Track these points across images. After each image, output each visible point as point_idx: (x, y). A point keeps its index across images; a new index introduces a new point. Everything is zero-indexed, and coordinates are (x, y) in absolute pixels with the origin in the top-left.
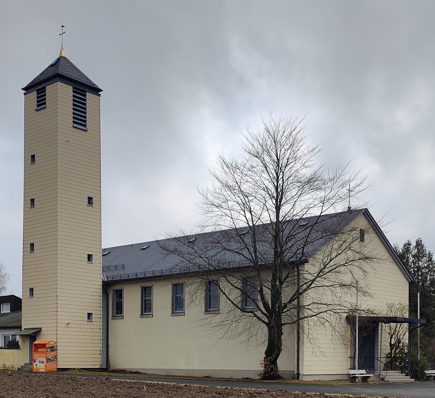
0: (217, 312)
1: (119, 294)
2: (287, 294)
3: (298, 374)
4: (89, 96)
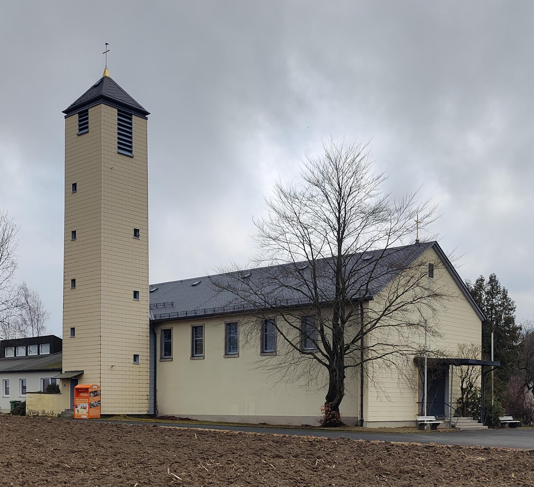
0: (274, 353)
1: (168, 334)
2: (349, 334)
4: (136, 119)
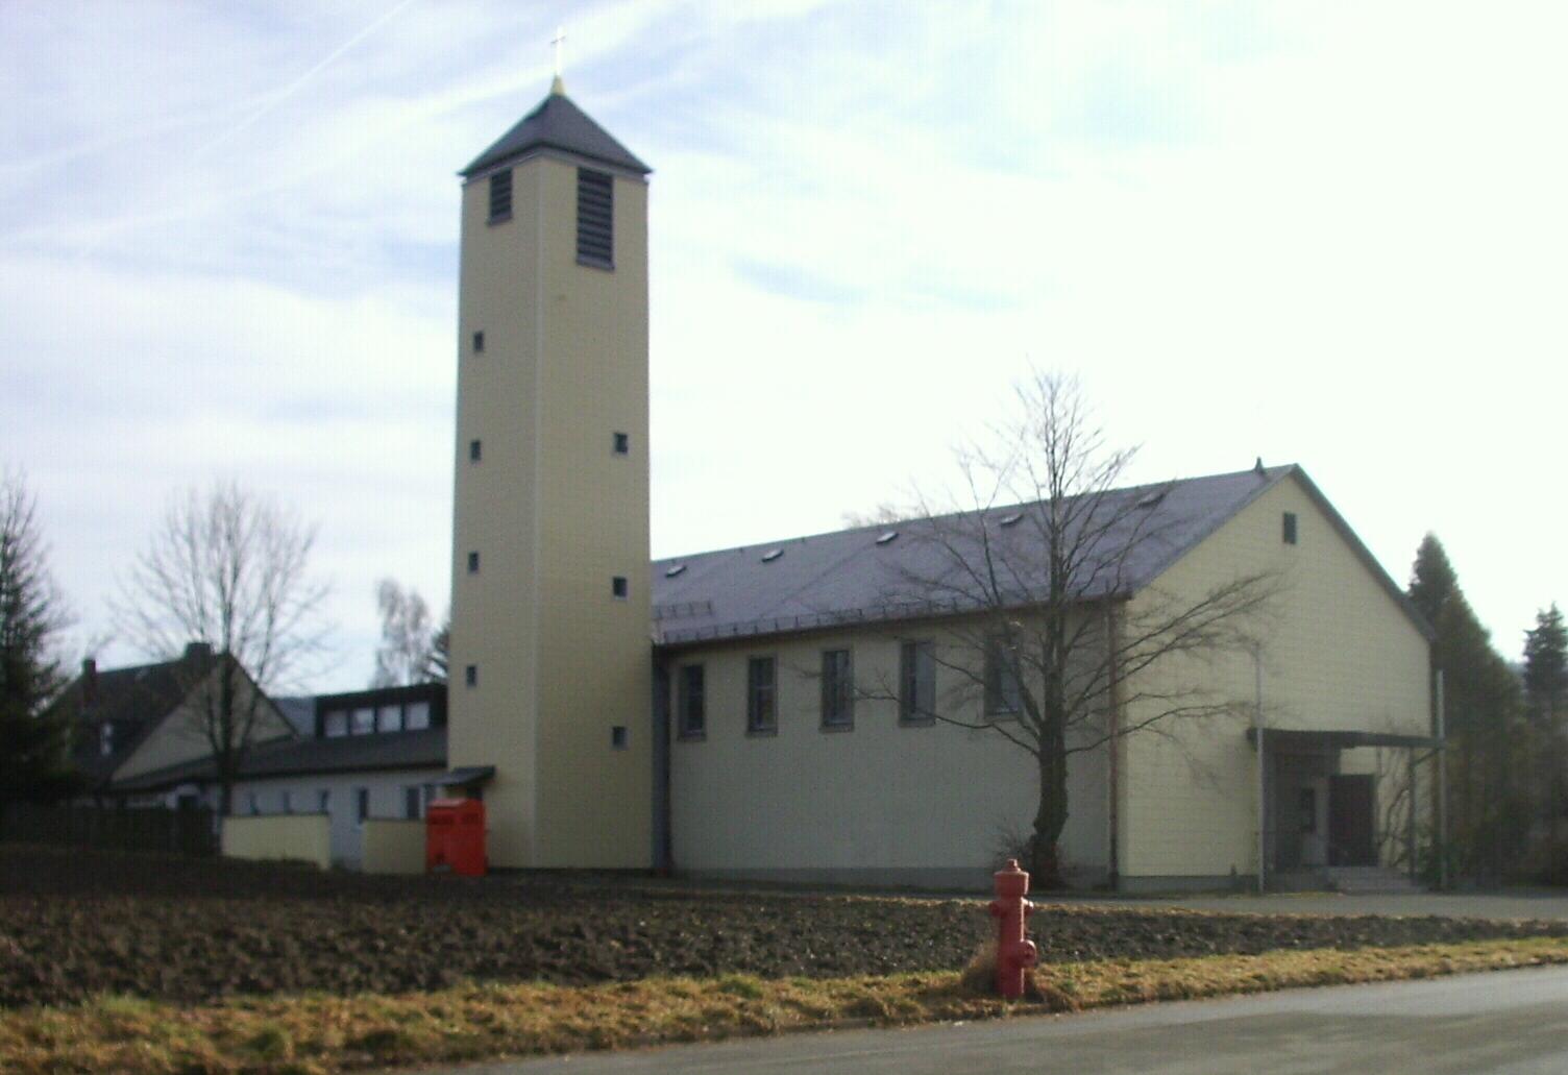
0: (931, 718)
1: (696, 677)
2: (1076, 679)
3: (1115, 875)
4: (621, 188)
